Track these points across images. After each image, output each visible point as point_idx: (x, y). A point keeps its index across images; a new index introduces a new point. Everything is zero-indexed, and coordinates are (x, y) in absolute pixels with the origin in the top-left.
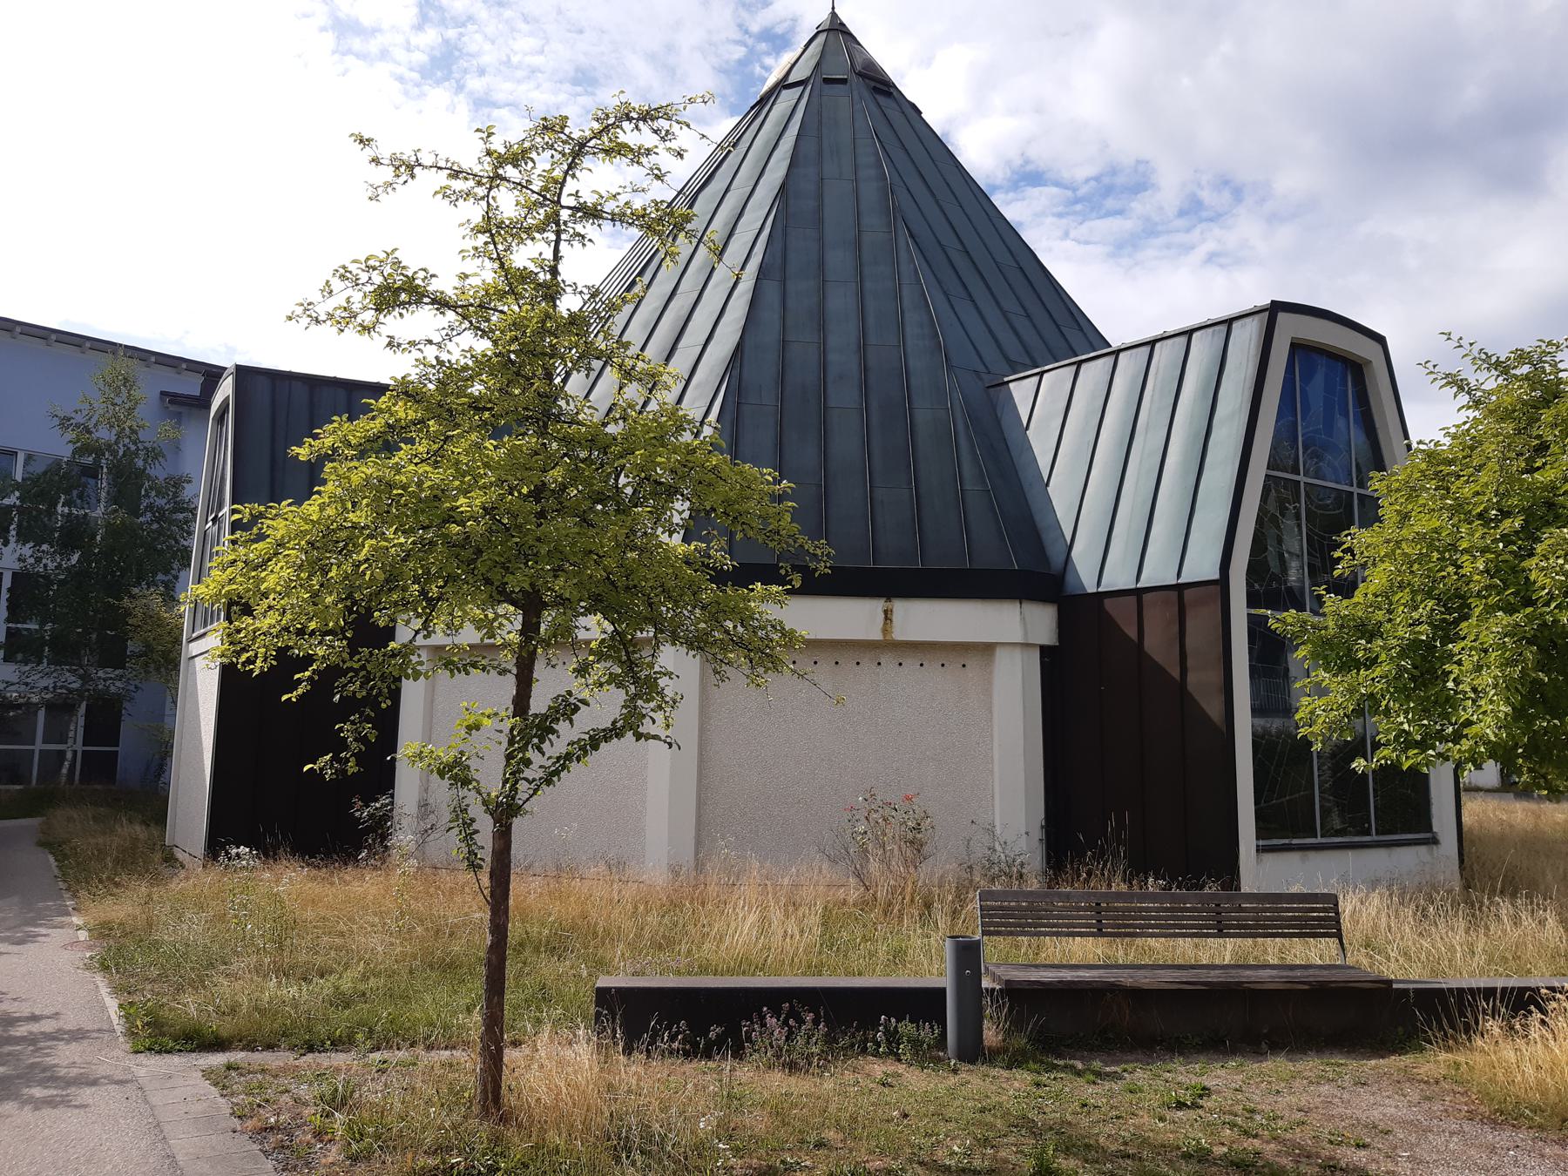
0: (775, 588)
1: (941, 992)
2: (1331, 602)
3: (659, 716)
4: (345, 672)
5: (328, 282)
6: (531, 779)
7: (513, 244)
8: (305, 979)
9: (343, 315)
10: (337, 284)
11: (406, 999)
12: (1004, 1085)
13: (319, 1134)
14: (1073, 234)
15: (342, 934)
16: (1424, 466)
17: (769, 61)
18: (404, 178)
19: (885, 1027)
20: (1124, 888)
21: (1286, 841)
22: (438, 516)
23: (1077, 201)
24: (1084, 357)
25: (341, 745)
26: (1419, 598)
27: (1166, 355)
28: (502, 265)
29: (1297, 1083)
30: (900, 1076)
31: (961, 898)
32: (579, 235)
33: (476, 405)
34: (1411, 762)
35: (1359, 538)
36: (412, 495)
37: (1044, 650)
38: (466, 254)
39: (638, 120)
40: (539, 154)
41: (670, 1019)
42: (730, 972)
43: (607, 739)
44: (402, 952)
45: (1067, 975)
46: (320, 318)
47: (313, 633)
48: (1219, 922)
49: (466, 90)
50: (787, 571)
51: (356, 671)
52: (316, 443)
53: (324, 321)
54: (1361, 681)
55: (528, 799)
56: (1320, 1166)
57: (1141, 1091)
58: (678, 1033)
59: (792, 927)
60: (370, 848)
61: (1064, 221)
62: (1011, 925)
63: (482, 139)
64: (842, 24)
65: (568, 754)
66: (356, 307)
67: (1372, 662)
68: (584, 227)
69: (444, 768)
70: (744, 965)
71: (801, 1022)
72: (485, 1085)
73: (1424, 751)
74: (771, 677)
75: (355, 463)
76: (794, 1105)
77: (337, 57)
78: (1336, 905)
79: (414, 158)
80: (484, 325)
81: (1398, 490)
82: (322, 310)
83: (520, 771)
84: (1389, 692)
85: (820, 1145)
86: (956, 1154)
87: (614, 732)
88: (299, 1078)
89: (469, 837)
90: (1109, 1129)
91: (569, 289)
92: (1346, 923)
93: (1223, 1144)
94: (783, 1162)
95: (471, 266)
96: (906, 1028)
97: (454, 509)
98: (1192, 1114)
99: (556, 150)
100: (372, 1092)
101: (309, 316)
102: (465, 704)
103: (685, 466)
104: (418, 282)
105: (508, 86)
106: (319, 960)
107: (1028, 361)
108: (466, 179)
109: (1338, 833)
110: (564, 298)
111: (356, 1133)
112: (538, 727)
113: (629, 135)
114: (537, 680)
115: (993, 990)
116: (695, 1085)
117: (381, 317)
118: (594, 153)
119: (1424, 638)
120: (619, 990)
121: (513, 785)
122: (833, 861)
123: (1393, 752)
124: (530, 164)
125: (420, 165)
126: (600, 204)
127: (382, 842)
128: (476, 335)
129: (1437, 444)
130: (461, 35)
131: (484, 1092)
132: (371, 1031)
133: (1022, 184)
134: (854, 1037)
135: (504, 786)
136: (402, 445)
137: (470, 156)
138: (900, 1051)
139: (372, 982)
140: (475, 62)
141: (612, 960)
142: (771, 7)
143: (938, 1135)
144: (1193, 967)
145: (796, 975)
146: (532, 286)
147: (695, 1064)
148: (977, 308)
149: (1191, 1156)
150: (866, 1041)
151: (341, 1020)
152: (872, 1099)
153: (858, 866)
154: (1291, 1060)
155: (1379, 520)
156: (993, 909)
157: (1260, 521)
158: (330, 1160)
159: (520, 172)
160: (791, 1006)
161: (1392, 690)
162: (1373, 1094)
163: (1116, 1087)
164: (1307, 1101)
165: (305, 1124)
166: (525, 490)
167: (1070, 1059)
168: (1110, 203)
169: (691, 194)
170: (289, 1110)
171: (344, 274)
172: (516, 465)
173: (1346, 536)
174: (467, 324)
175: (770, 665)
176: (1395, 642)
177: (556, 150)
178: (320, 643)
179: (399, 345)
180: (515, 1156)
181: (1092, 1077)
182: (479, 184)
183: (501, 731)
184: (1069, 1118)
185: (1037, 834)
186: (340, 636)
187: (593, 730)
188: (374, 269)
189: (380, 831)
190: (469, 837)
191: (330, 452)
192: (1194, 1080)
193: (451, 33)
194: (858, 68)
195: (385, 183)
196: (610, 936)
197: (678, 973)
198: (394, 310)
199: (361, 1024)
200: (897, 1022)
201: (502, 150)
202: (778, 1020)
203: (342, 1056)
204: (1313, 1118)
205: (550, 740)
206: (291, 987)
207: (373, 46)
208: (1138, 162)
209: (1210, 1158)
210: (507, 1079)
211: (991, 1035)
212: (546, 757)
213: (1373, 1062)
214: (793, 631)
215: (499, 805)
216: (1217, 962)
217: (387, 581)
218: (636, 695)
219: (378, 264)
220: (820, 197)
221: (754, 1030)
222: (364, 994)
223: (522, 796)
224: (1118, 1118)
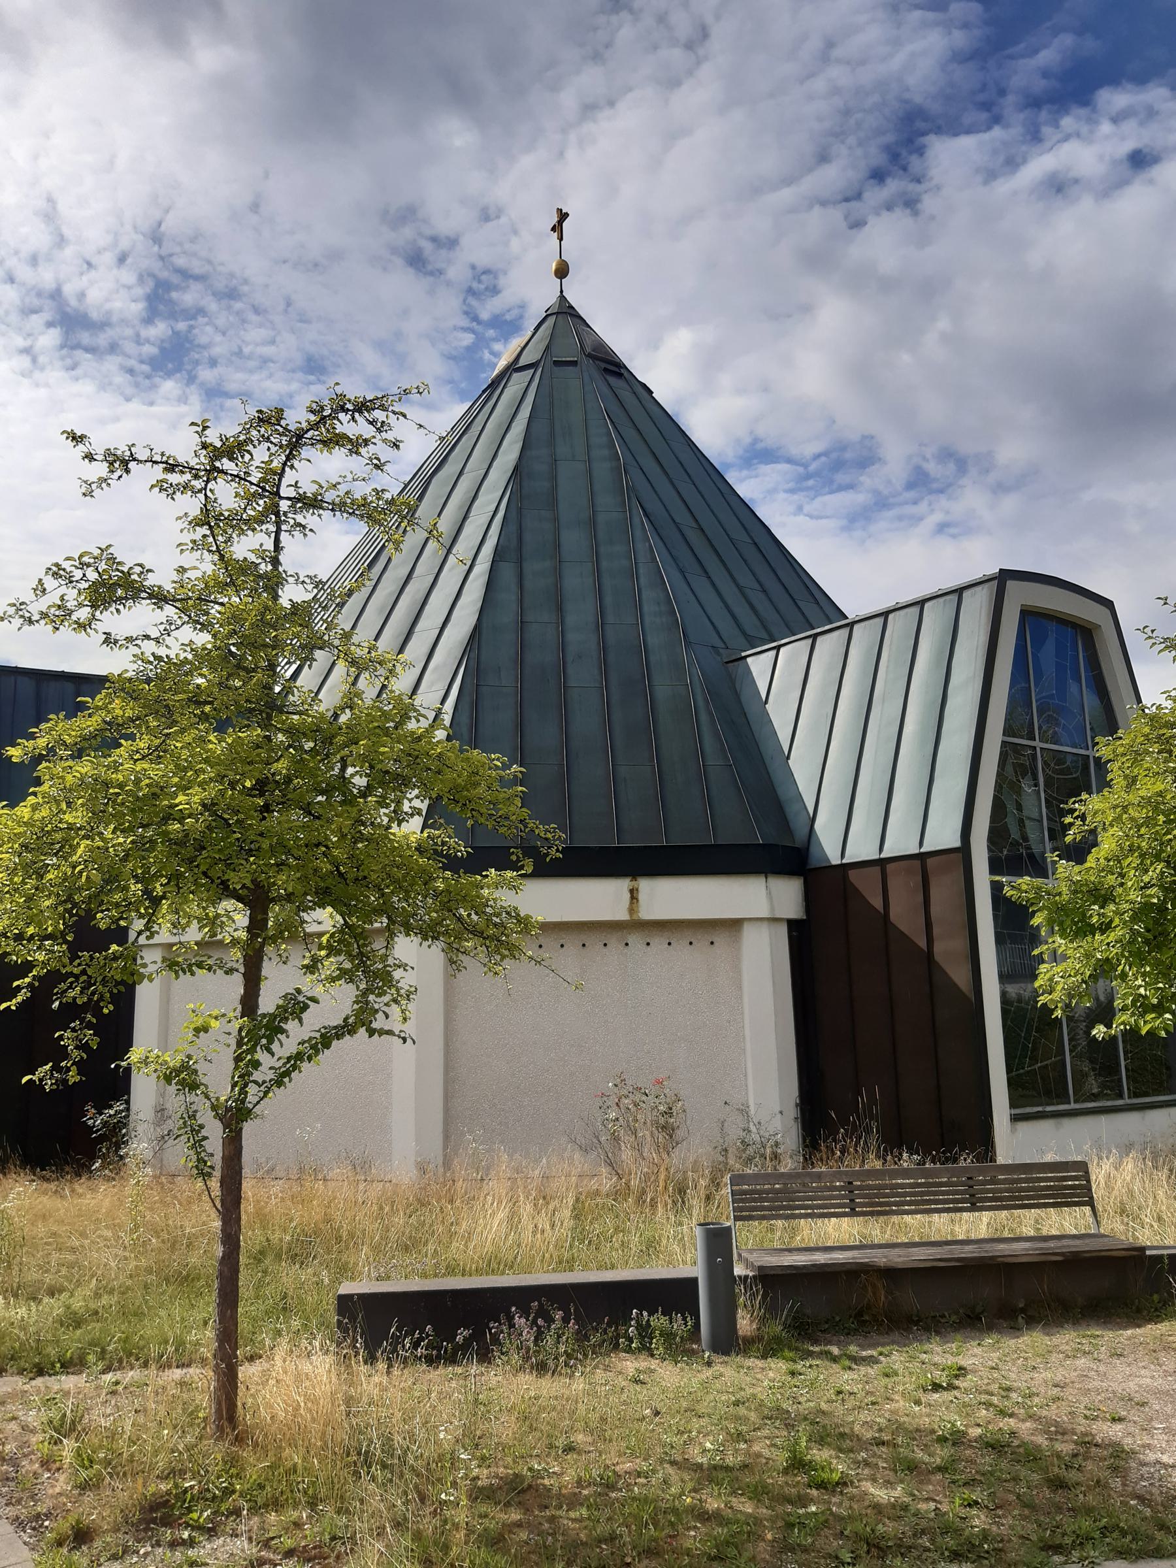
0: (509, 874)
1: (694, 1281)
2: (1065, 868)
3: (395, 1010)
4: (64, 978)
5: (40, 580)
6: (260, 1082)
7: (234, 535)
8: (34, 1299)
9: (57, 613)
10: (50, 583)
11: (139, 1314)
12: (759, 1376)
13: (46, 1463)
14: (807, 509)
15: (73, 1250)
16: (1147, 730)
17: (497, 347)
18: (119, 473)
19: (637, 1322)
20: (878, 1164)
21: (1040, 1109)
22: (157, 814)
23: (808, 477)
24: (819, 630)
25: (64, 1053)
26: (1149, 862)
27: (935, 619)
28: (222, 557)
29: (1054, 1358)
30: (653, 1371)
31: (716, 1183)
32: (300, 525)
33: (196, 700)
34: (1148, 1027)
35: (1094, 804)
36: (128, 793)
37: (792, 924)
38: (184, 547)
39: (353, 411)
40: (255, 447)
41: (412, 1324)
42: (479, 1272)
43: (339, 1037)
44: (136, 1266)
45: (821, 1258)
46: (34, 618)
47: (32, 937)
48: (972, 1195)
49: (198, 381)
50: (518, 857)
51: (77, 977)
52: (30, 744)
53: (37, 621)
54: (1096, 945)
55: (258, 1102)
56: (1076, 1443)
57: (897, 1374)
58: (421, 1339)
59: (543, 1222)
60: (104, 1157)
61: (796, 497)
62: (763, 1208)
63: (197, 432)
64: (572, 307)
65: (299, 1054)
66: (71, 604)
67: (1106, 927)
68: (305, 517)
69: (171, 1073)
70: (493, 1264)
71: (550, 1320)
72: (219, 1403)
73: (1161, 1015)
74: (508, 963)
75: (70, 763)
76: (542, 1409)
77: (65, 352)
78: (1087, 1172)
79: (128, 453)
80: (203, 619)
81: (1124, 755)
82: (37, 607)
83: (249, 1074)
84: (1123, 956)
85: (569, 1449)
86: (709, 1451)
87: (346, 1029)
88: (27, 1404)
89: (198, 1144)
90: (864, 1416)
91: (291, 580)
92: (1098, 1192)
93: (979, 1425)
94: (530, 1469)
95: (189, 559)
96: (659, 1321)
97: (173, 806)
98: (947, 1396)
99: (271, 442)
100: (100, 1417)
101: (22, 617)
102: (191, 1006)
103: (410, 755)
104: (135, 577)
105: (239, 376)
106: (48, 1279)
107: (765, 636)
108: (182, 472)
109: (1095, 1097)
110: (287, 588)
111: (84, 1460)
112: (267, 1027)
113: (346, 425)
114: (266, 978)
115: (746, 1277)
116: (440, 1393)
117: (98, 613)
118: (312, 444)
119: (1155, 901)
120: (362, 1297)
121: (241, 1089)
122: (585, 1150)
123: (1131, 1017)
124: (247, 457)
125: (134, 460)
126: (321, 494)
127: (116, 1151)
128: (195, 629)
129: (1159, 707)
130: (191, 327)
131: (219, 1411)
132: (103, 1351)
133: (755, 461)
134: (606, 1333)
135: (232, 1089)
136: (122, 741)
137: (184, 448)
138: (653, 1346)
139: (105, 1300)
140: (206, 354)
141: (356, 1264)
142: (500, 295)
143: (690, 1432)
144: (948, 1243)
145: (548, 1271)
146: (251, 579)
147: (441, 1371)
148: (714, 585)
149: (945, 1440)
150: (618, 1337)
151: (72, 1341)
152: (624, 1397)
153: (610, 1155)
154: (1048, 1335)
155: (1108, 784)
156: (745, 1193)
157: (999, 787)
158: (58, 1490)
159: (237, 465)
160: (541, 1305)
161: (1126, 954)
162: (1129, 1365)
163: (872, 1371)
164: (1063, 1375)
165: (32, 1453)
166: (248, 784)
167: (826, 1345)
168: (841, 478)
169: (424, 480)
170: (15, 1439)
171: (57, 572)
172: (238, 758)
173: (1074, 803)
174: (186, 619)
175: (506, 953)
176: (1126, 906)
177: (271, 442)
178: (39, 948)
179: (116, 642)
180: (251, 1477)
181: (847, 1363)
182: (196, 477)
183: (229, 1034)
184: (824, 1406)
185: (792, 1112)
186: (60, 941)
187: (325, 1028)
188: (89, 565)
189: (114, 1140)
190: (198, 1144)
191: (44, 753)
192: (950, 1360)
193: (182, 326)
194: (588, 350)
195: (99, 479)
196: (354, 1239)
197: (424, 1275)
198: (110, 606)
199: (93, 1344)
200: (649, 1316)
201: (218, 444)
202: (528, 1320)
203: (72, 1378)
204: (1070, 1393)
205: (279, 1040)
206: (20, 1307)
207: (102, 339)
208: (864, 437)
209: (965, 1440)
210: (243, 1397)
211: (745, 1324)
212: (276, 1057)
213: (1129, 1332)
214: (528, 917)
215: (228, 1109)
216: (973, 1236)
217: (107, 882)
218: (367, 990)
219: (92, 561)
220: (554, 478)
221: (502, 1332)
222: (96, 1313)
223: (251, 1099)
224: (873, 1403)
